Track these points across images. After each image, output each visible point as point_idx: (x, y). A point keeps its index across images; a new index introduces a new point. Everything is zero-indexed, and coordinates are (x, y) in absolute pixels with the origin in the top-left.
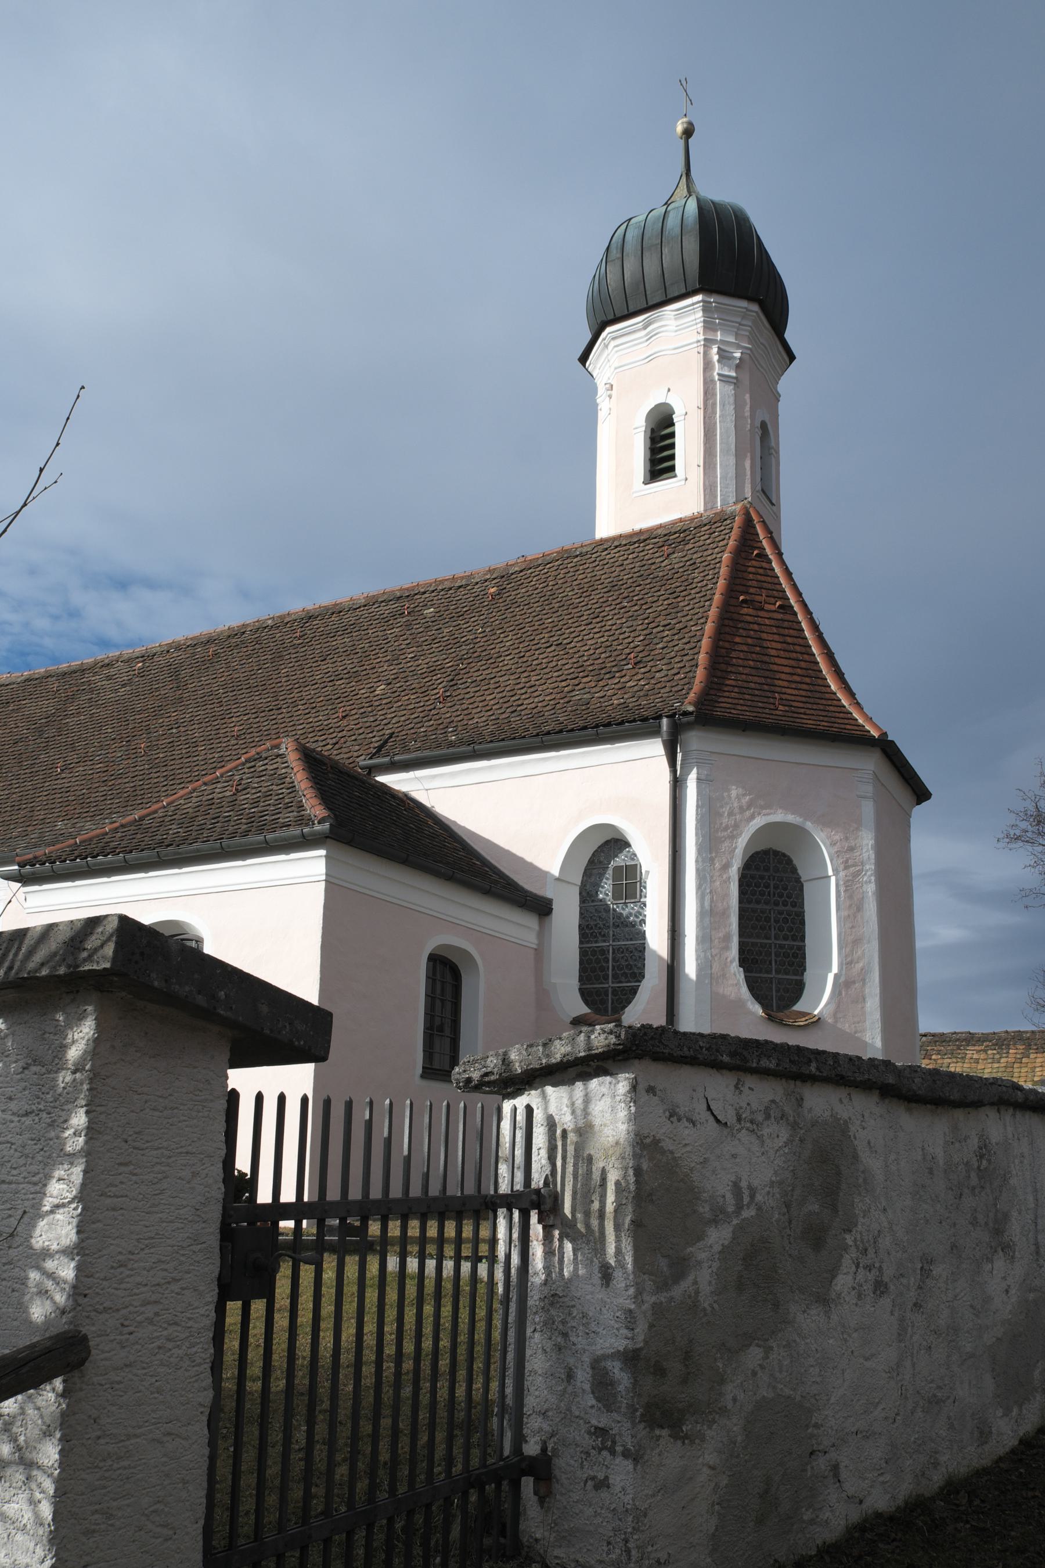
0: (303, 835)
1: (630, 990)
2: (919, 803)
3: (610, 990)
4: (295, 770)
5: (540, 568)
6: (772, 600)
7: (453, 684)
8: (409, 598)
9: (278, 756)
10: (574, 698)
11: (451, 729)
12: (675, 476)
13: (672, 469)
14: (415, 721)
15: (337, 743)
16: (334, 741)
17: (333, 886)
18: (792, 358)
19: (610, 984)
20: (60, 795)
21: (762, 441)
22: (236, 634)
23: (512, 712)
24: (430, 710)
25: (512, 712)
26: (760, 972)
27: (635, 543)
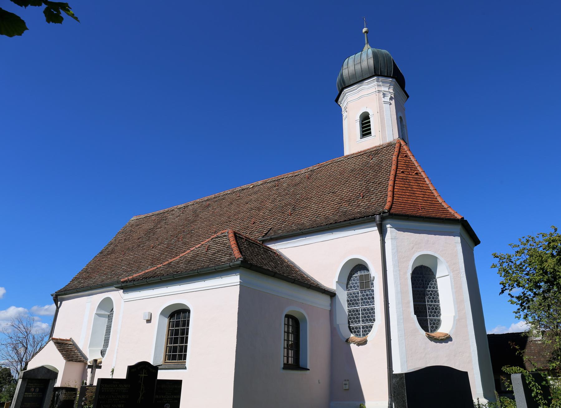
0: (230, 266)
1: (370, 326)
2: (476, 245)
3: (361, 327)
5: (325, 167)
6: (413, 171)
7: (294, 209)
8: (278, 181)
9: (224, 236)
10: (340, 211)
12: (371, 135)
13: (370, 133)
14: (280, 223)
15: (251, 233)
16: (250, 232)
17: (242, 286)
18: (408, 96)
19: (361, 324)
20: (151, 257)
21: (400, 123)
22: (217, 197)
23: (317, 217)
24: (286, 219)
25: (317, 217)
26: (423, 316)
27: (359, 155)
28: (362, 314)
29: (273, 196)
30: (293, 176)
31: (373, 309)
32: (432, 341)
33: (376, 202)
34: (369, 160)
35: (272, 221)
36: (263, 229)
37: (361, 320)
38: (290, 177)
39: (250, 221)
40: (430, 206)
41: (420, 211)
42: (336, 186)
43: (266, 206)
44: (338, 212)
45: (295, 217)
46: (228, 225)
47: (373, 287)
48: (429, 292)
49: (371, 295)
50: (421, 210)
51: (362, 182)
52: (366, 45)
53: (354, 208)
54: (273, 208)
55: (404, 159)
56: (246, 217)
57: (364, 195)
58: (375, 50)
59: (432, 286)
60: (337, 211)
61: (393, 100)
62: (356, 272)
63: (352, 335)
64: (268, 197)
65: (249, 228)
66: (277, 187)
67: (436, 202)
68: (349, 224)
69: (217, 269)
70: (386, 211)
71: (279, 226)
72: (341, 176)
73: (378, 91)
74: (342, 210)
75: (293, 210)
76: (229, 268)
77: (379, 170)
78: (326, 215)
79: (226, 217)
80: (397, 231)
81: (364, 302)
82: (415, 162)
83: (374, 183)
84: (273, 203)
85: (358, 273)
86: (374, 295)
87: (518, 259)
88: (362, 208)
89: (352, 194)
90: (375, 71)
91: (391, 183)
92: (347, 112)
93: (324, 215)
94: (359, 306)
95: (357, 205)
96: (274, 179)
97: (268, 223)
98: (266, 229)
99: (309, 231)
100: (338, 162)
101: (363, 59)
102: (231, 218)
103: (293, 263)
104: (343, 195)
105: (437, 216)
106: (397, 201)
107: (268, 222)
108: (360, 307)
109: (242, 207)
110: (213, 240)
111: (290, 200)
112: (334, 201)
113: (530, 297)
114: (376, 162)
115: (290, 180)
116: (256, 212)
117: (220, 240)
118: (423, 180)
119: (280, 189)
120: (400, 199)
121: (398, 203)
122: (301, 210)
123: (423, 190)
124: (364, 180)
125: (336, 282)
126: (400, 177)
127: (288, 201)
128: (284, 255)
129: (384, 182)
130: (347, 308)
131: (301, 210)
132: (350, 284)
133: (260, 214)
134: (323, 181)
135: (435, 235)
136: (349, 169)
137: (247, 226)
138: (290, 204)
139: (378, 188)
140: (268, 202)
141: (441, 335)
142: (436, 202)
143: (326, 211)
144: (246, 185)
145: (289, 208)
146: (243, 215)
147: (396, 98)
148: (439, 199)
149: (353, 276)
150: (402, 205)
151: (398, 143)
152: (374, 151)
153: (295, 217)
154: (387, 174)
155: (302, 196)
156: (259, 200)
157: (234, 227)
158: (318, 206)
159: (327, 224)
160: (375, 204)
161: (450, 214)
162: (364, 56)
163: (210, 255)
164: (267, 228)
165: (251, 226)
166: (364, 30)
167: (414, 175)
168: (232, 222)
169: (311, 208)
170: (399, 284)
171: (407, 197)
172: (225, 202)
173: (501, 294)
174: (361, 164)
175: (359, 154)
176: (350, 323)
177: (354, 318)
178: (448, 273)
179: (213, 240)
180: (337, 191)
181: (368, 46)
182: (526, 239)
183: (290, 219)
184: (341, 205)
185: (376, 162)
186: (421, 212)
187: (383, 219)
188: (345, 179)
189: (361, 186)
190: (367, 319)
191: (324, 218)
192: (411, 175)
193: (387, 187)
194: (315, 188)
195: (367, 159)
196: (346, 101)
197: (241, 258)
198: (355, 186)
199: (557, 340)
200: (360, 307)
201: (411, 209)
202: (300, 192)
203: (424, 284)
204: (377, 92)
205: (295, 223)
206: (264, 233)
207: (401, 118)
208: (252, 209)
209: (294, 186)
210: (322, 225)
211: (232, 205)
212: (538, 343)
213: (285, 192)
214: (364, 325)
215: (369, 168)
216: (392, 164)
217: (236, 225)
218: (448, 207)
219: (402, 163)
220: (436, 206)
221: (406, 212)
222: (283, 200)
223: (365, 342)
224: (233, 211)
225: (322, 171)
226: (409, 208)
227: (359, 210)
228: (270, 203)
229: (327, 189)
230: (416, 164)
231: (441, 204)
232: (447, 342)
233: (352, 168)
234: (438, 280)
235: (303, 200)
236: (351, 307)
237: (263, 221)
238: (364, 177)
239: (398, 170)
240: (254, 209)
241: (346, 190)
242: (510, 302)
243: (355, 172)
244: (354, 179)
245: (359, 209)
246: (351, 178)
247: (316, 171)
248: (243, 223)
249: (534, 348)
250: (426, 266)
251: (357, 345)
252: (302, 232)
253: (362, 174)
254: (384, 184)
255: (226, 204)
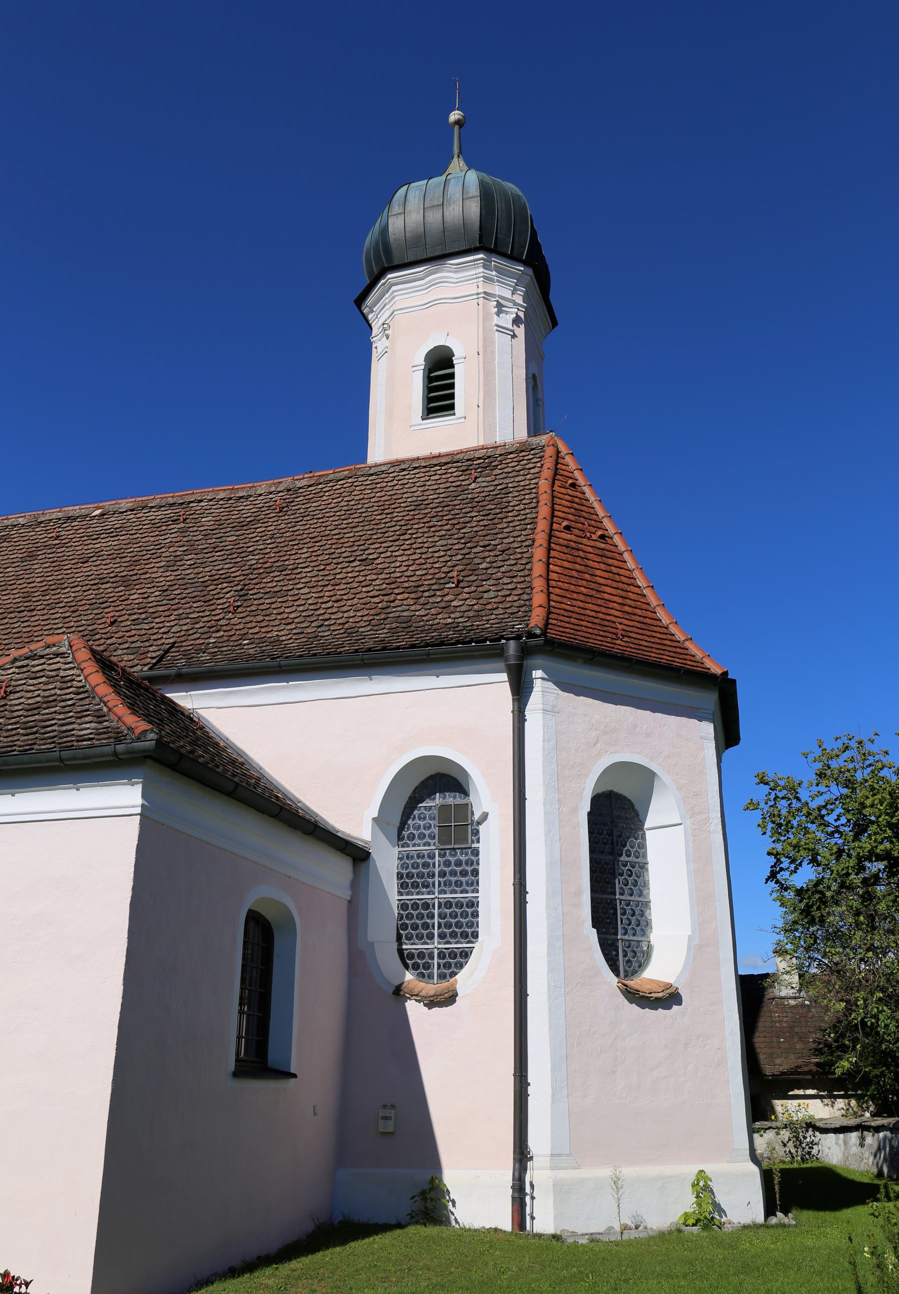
0: (115, 754)
1: (461, 953)
4: (86, 672)
5: (331, 484)
6: (593, 530)
7: (242, 595)
8: (184, 506)
9: (57, 655)
10: (391, 615)
11: (246, 642)
12: (454, 414)
13: (451, 407)
18: (555, 323)
19: (436, 944)
27: (436, 465)
28: (440, 916)
29: (171, 550)
30: (230, 499)
31: (473, 904)
32: (631, 1003)
33: (500, 603)
34: (467, 482)
35: (173, 623)
36: (147, 644)
37: (436, 932)
38: (222, 499)
39: (99, 616)
40: (640, 631)
41: (619, 642)
42: (370, 542)
43: (148, 575)
44: (385, 619)
45: (248, 619)
46: (26, 619)
47: (478, 842)
48: (625, 866)
49: (470, 863)
50: (621, 640)
51: (450, 542)
52: (455, 159)
53: (433, 611)
54: (173, 583)
55: (569, 491)
56: (84, 602)
57: (461, 578)
58: (487, 178)
59: (633, 851)
60: (383, 616)
61: (522, 326)
62: (430, 795)
63: (409, 976)
64: (154, 551)
65: (98, 637)
66: (182, 525)
67: (655, 623)
68: (425, 657)
69: (69, 759)
70: (538, 632)
71: (198, 638)
72: (384, 516)
73: (485, 293)
74: (397, 614)
75: (241, 596)
76: (112, 758)
77: (501, 513)
78: (348, 622)
79: (17, 596)
80: (560, 692)
81: (448, 884)
82: (596, 505)
83: (488, 548)
84: (172, 568)
85: (435, 799)
86: (478, 864)
87: (819, 792)
88: (457, 615)
89: (424, 572)
90: (481, 236)
91: (539, 553)
92: (387, 338)
93: (340, 621)
94: (434, 894)
95: (443, 604)
96: (171, 501)
97: (160, 628)
98: (155, 643)
99: (304, 664)
100: (372, 475)
101: (451, 197)
102: (34, 599)
103: (240, 753)
104: (395, 572)
105: (662, 661)
106: (558, 605)
107: (161, 625)
108: (437, 895)
109: (69, 572)
110: (18, 664)
111: (227, 566)
112: (368, 586)
113: (829, 894)
114: (488, 489)
115: (223, 510)
116: (117, 590)
117: (45, 666)
118: (618, 558)
119: (191, 529)
120: (565, 601)
121: (562, 612)
122: (267, 601)
123: (621, 585)
124: (456, 536)
125: (373, 819)
126: (561, 541)
127: (222, 569)
128: (217, 730)
129: (518, 550)
130: (397, 897)
131: (267, 601)
132: (408, 829)
133: (131, 597)
134: (328, 523)
135: (654, 711)
136: (409, 500)
137: (90, 628)
138: (227, 579)
139: (502, 563)
140: (157, 565)
141: (654, 988)
142: (655, 623)
143: (347, 611)
144: (78, 507)
145: (224, 591)
146: (73, 595)
147: (527, 321)
148: (661, 614)
149: (420, 805)
150: (572, 619)
151: (553, 445)
152: (479, 458)
153: (248, 619)
154: (525, 527)
155: (266, 560)
156: (125, 555)
157: (46, 628)
158: (321, 594)
159: (356, 651)
160: (497, 608)
161: (693, 658)
162: (454, 190)
163: (21, 713)
164: (160, 642)
165: (103, 631)
166: (454, 116)
167: (596, 540)
168: (39, 613)
169: (296, 598)
170: (558, 838)
171: (582, 597)
172: (9, 549)
173: (769, 882)
174: (444, 490)
175: (435, 462)
176: (404, 940)
177: (415, 927)
178: (681, 819)
179: (18, 664)
180: (375, 556)
181: (462, 163)
182: (844, 744)
183: (232, 621)
184: (392, 597)
185: (488, 489)
186: (620, 646)
187: (526, 652)
188: (398, 528)
189: (449, 553)
190: (454, 931)
191: (342, 631)
192: (589, 539)
193: (527, 563)
194: (305, 541)
195: (461, 478)
196: (387, 307)
197: (152, 730)
198: (430, 550)
199: (859, 1003)
200: (435, 897)
201: (596, 632)
202: (259, 547)
203: (615, 845)
204: (482, 295)
205: (251, 636)
206: (149, 655)
207: (534, 376)
208: (102, 581)
209: (238, 528)
210: (342, 650)
211: (36, 562)
212: (788, 1004)
213: (209, 541)
214: (445, 949)
215: (470, 505)
216: (538, 502)
217: (53, 622)
218: (687, 640)
219: (564, 502)
220: (656, 632)
221: (586, 640)
222: (203, 565)
223: (449, 999)
224: (38, 580)
225: (322, 494)
226: (590, 630)
227: (449, 620)
228: (162, 570)
229: (344, 550)
230: (601, 513)
231: (667, 628)
232: (669, 1008)
233: (415, 499)
234: (649, 835)
235: (268, 570)
236: (407, 894)
237: (144, 619)
238: (457, 527)
239: (555, 519)
240: (111, 580)
241: (405, 558)
242: (778, 903)
243: (426, 511)
244: (426, 530)
245: (450, 617)
246: (416, 526)
247: (305, 494)
248: (75, 619)
249: (779, 1017)
250: (621, 795)
251: (425, 1005)
252: (280, 666)
253: (448, 517)
254: (519, 556)
255: (14, 556)
